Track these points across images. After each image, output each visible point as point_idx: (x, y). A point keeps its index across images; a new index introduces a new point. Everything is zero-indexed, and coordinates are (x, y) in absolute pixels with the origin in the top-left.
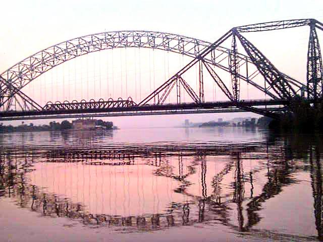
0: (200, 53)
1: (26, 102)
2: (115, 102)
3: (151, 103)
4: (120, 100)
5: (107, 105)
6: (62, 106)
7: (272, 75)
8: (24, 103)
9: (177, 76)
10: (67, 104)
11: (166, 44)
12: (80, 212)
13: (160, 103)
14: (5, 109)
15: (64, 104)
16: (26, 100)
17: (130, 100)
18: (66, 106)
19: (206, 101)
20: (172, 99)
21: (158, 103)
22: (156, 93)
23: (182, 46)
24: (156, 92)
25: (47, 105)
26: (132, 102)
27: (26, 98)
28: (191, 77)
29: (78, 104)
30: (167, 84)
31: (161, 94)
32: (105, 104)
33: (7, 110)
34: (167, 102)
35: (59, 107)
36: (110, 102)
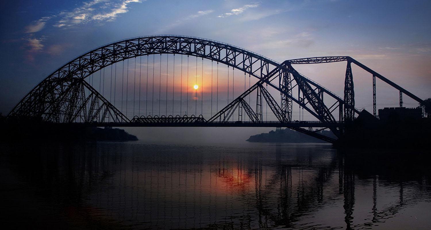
0: (278, 73)
1: (118, 116)
2: (189, 118)
3: (218, 120)
4: (193, 116)
5: (190, 121)
6: (145, 120)
7: (111, 57)
8: (115, 117)
9: (240, 99)
10: (144, 118)
11: (215, 54)
12: (139, 186)
13: (226, 120)
14: (63, 122)
15: (147, 118)
16: (117, 114)
17: (201, 117)
18: (149, 120)
19: (264, 120)
20: (234, 118)
21: (224, 120)
22: (222, 113)
23: (249, 65)
24: (222, 112)
25: (134, 119)
26: (203, 119)
27: (118, 112)
28: (251, 100)
29: (159, 118)
30: (232, 105)
31: (226, 113)
32: (188, 119)
33: (102, 121)
34: (230, 120)
35: (143, 121)
36: (185, 118)
